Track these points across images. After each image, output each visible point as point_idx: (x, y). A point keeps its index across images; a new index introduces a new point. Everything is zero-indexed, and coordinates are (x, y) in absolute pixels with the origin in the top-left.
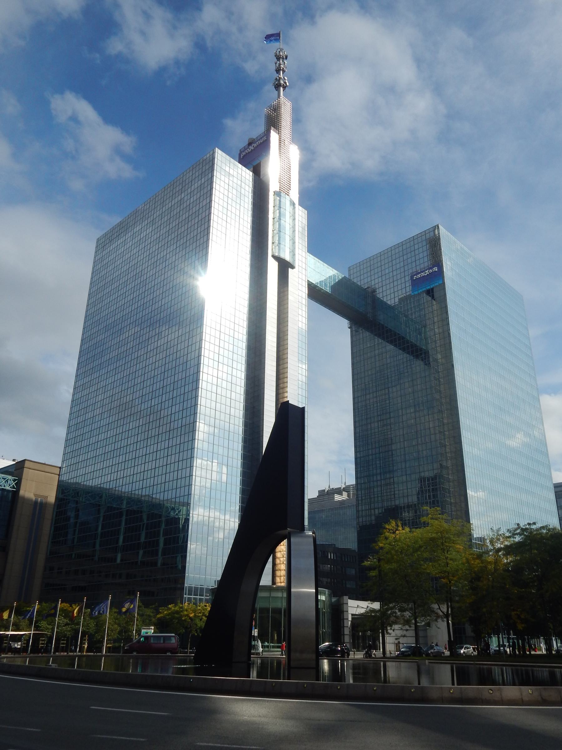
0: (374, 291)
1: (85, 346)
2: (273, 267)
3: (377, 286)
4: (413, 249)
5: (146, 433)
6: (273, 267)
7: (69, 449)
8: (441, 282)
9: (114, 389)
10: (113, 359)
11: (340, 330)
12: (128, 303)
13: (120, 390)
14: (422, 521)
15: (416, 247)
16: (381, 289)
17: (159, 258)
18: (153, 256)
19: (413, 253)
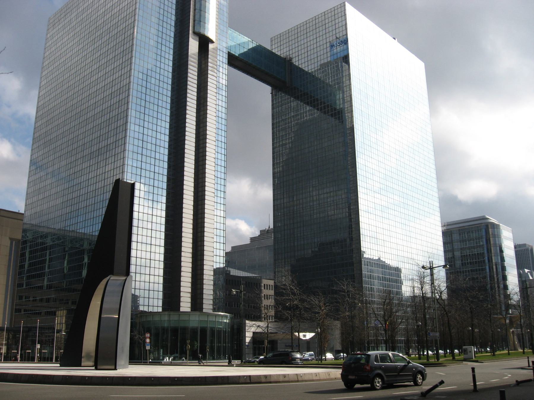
0: (291, 59)
1: (40, 113)
2: (193, 45)
3: (294, 56)
4: (324, 23)
5: (103, 182)
6: (193, 45)
7: (30, 201)
8: (119, 164)
9: (102, 130)
10: (107, 97)
11: (262, 93)
12: (129, 38)
13: (107, 131)
14: (59, 313)
15: (327, 21)
16: (297, 58)
17: (128, 13)
18: (123, 11)
19: (324, 27)
